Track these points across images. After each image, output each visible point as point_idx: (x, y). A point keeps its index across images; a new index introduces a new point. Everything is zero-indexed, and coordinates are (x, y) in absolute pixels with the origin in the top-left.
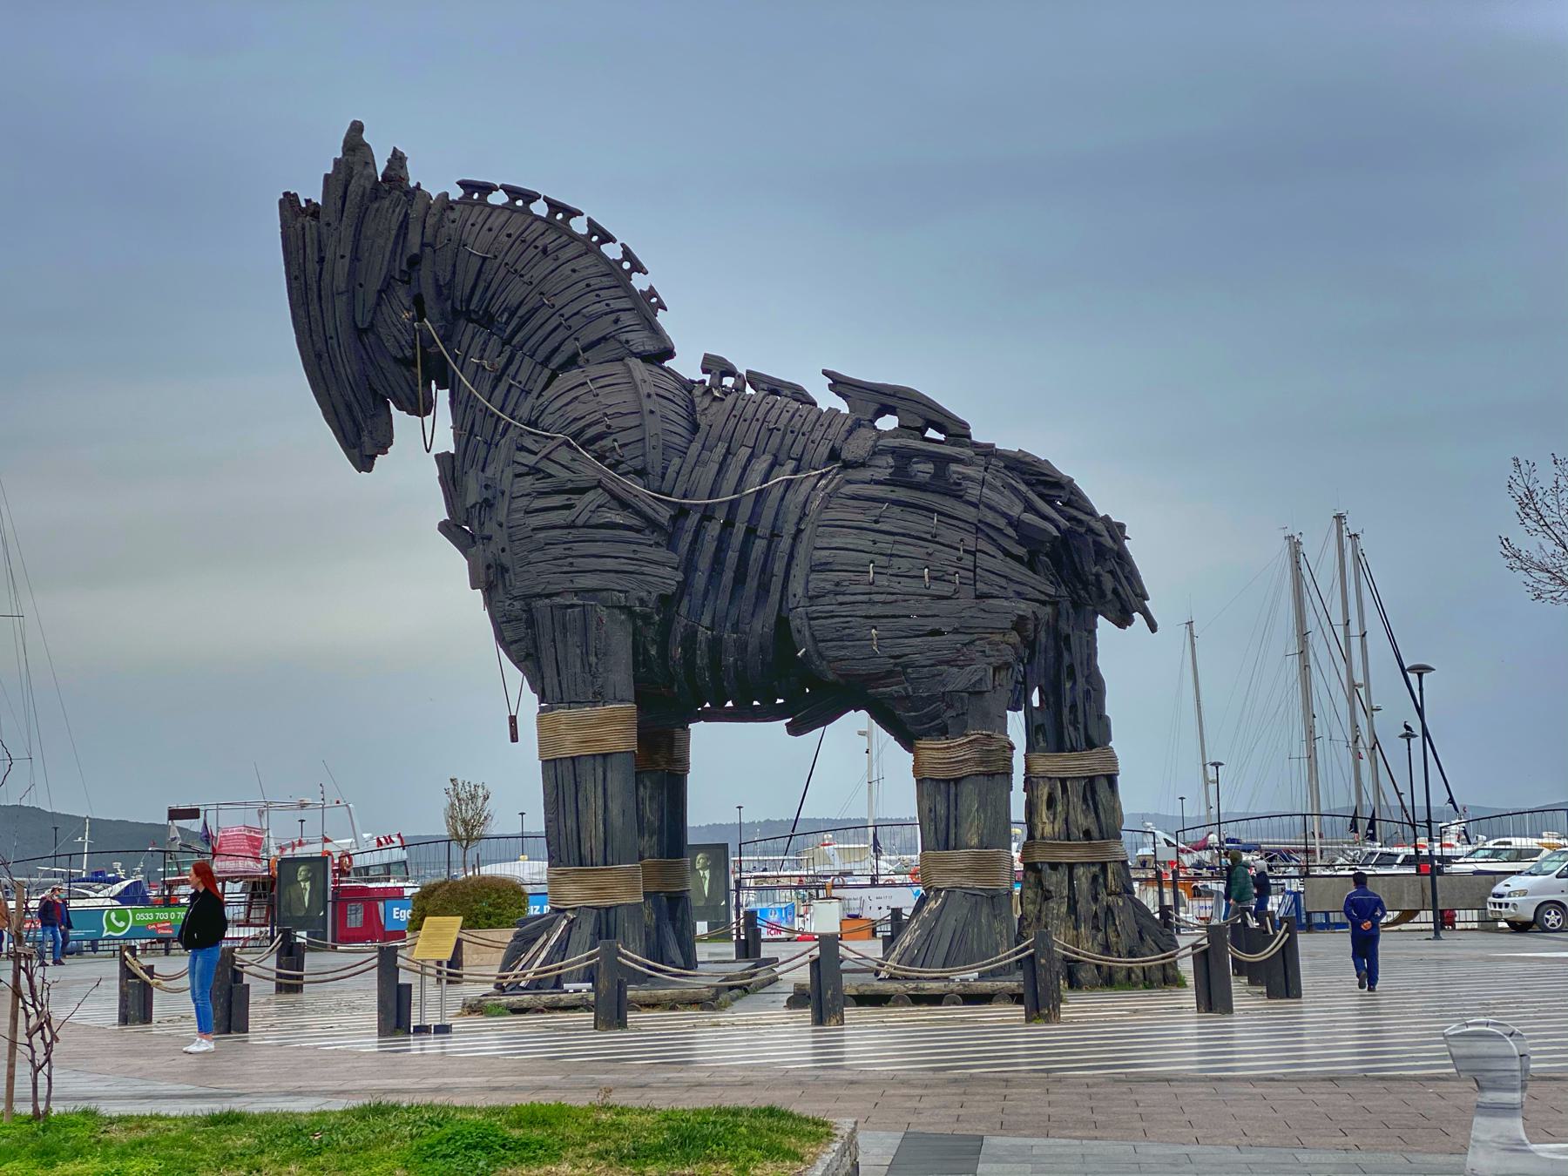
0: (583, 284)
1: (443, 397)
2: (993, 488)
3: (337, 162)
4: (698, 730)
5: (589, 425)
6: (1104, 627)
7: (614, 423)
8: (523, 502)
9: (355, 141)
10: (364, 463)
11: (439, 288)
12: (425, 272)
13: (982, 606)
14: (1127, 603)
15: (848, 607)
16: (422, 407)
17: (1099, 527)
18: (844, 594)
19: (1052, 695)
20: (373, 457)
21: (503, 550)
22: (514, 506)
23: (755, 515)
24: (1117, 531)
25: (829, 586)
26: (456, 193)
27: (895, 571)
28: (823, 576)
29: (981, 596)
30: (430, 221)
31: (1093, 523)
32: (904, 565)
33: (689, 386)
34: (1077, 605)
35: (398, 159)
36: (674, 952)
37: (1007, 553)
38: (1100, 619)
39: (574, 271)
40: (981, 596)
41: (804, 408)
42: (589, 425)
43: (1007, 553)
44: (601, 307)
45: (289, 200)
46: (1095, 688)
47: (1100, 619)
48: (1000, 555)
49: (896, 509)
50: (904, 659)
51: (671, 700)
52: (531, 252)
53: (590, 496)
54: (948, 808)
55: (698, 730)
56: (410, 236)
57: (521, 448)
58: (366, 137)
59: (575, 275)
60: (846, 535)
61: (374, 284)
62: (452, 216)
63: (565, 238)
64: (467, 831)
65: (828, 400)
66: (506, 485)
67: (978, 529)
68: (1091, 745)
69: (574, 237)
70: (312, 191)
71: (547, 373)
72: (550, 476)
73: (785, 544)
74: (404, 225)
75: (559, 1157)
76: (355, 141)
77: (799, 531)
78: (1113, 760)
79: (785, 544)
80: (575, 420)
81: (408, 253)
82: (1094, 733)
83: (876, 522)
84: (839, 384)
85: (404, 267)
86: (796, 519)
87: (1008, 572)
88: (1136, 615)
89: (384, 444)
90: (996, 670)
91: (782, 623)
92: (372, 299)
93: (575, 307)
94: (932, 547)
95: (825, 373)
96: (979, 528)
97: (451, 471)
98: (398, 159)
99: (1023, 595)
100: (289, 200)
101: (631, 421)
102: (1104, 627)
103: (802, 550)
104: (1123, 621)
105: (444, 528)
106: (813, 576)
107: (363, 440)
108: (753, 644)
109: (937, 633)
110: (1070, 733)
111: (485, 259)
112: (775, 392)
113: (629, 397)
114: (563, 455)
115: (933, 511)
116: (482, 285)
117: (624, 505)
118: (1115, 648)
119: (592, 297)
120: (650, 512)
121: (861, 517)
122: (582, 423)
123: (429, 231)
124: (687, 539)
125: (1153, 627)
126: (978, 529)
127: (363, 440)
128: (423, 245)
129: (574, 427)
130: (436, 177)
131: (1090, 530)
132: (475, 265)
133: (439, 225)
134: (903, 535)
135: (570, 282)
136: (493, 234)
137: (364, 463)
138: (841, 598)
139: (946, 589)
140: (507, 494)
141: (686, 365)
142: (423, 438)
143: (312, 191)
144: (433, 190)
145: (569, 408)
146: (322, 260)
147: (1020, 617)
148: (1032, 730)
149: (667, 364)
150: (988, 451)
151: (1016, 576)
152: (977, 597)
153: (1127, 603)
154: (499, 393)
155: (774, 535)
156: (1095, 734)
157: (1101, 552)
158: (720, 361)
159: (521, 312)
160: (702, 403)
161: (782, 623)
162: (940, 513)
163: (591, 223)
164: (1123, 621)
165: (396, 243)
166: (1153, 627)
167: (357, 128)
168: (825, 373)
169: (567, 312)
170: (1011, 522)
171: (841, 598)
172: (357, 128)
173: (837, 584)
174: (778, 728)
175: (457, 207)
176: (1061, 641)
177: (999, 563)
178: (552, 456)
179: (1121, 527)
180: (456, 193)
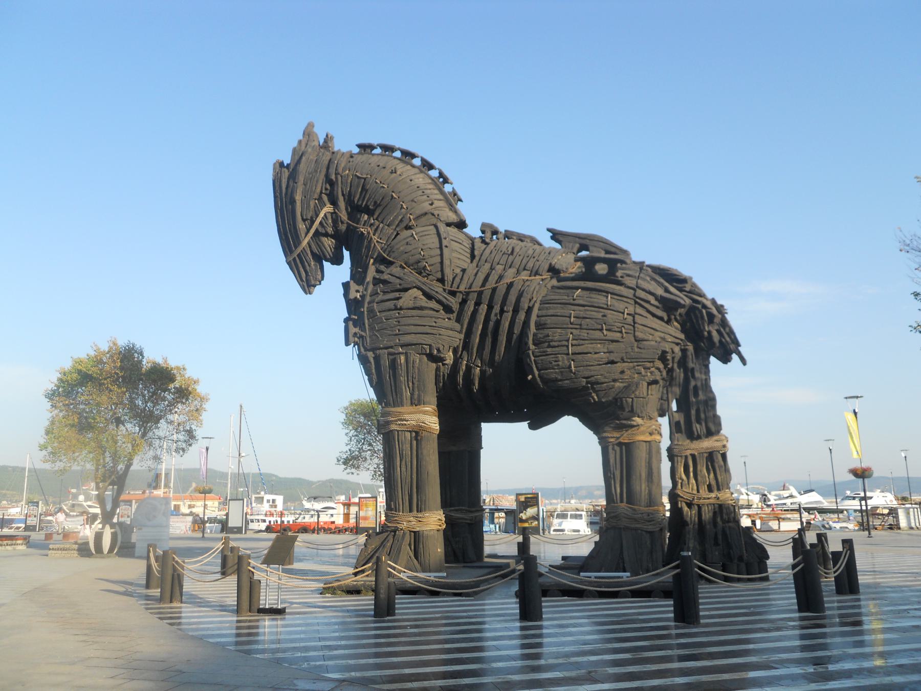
1: (346, 254)
2: (644, 280)
4: (485, 426)
6: (714, 363)
14: (727, 348)
17: (709, 304)
19: (684, 405)
24: (720, 309)
26: (356, 150)
31: (704, 301)
33: (472, 240)
34: (697, 350)
37: (654, 315)
38: (713, 359)
41: (536, 246)
46: (710, 402)
47: (713, 359)
50: (592, 379)
51: (467, 408)
54: (622, 466)
55: (485, 426)
60: (555, 308)
65: (547, 242)
68: (710, 433)
76: (308, 133)
82: (713, 428)
84: (556, 236)
90: (649, 384)
95: (549, 230)
96: (637, 301)
98: (328, 139)
99: (668, 336)
102: (714, 363)
104: (725, 359)
110: (697, 428)
115: (607, 292)
118: (721, 377)
120: (444, 300)
125: (744, 362)
126: (636, 302)
127: (308, 283)
130: (345, 144)
131: (704, 306)
141: (474, 230)
144: (344, 150)
148: (675, 428)
149: (464, 230)
150: (641, 265)
153: (727, 348)
156: (713, 427)
157: (711, 317)
160: (479, 245)
162: (612, 294)
164: (725, 359)
166: (744, 362)
167: (310, 125)
168: (549, 230)
175: (355, 156)
176: (689, 374)
179: (722, 306)
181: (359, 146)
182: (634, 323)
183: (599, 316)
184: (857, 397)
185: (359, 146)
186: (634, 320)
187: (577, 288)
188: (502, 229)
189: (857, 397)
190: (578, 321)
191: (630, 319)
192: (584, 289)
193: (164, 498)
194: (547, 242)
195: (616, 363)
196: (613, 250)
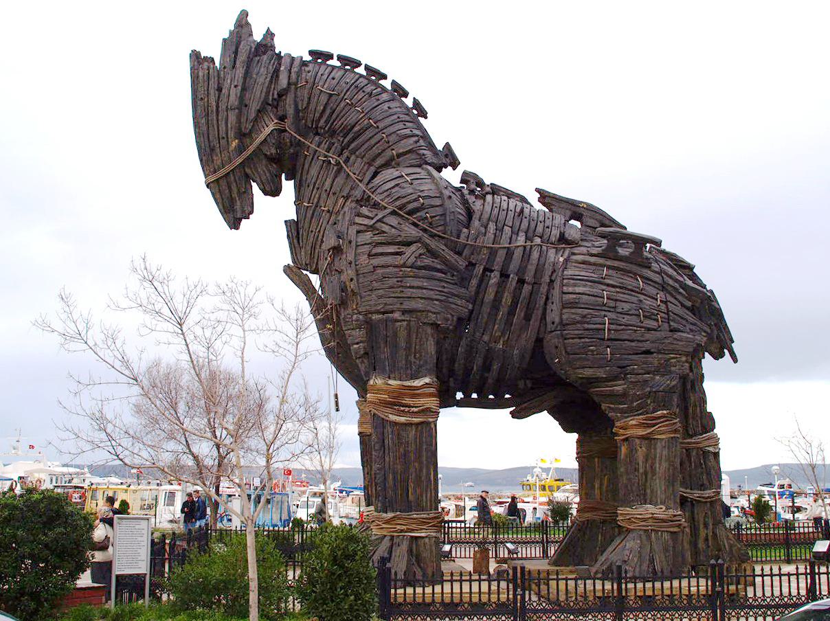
0: (396, 117)
3: (231, 33)
5: (409, 202)
8: (366, 249)
9: (242, 23)
10: (234, 224)
11: (297, 111)
12: (289, 99)
13: (675, 336)
15: (591, 332)
16: (273, 190)
18: (588, 323)
20: (240, 220)
21: (352, 280)
22: (359, 251)
23: (522, 270)
25: (578, 318)
26: (307, 58)
27: (620, 310)
28: (573, 311)
29: (673, 330)
30: (294, 70)
32: (626, 307)
35: (269, 35)
39: (389, 108)
40: (673, 330)
42: (409, 202)
43: (683, 305)
44: (407, 132)
45: (196, 56)
48: (679, 305)
52: (361, 95)
53: (413, 248)
55: (546, 412)
56: (281, 77)
57: (359, 215)
58: (249, 19)
61: (254, 106)
62: (307, 69)
63: (379, 89)
64: (167, 441)
65: (533, 198)
66: (353, 238)
69: (384, 89)
70: (213, 50)
72: (384, 232)
73: (544, 289)
74: (276, 72)
76: (242, 23)
77: (552, 281)
78: (716, 441)
79: (544, 289)
81: (279, 88)
84: (544, 197)
85: (276, 96)
86: (550, 274)
89: (248, 213)
91: (539, 341)
92: (252, 115)
93: (391, 129)
94: (642, 297)
97: (295, 231)
98: (269, 35)
100: (196, 56)
101: (438, 202)
103: (556, 292)
105: (287, 270)
106: (565, 311)
107: (235, 210)
108: (161, 373)
109: (648, 352)
111: (331, 95)
113: (433, 187)
114: (393, 221)
116: (328, 112)
119: (401, 126)
121: (593, 275)
122: (404, 201)
123: (294, 76)
124: (474, 282)
125: (735, 360)
127: (235, 210)
128: (289, 84)
129: (398, 203)
132: (324, 99)
133: (299, 74)
134: (620, 288)
135: (388, 113)
136: (335, 82)
137: (234, 224)
138: (586, 326)
139: (651, 324)
140: (353, 244)
142: (275, 210)
143: (213, 50)
145: (393, 191)
146: (220, 90)
147: (698, 345)
152: (671, 331)
155: (536, 283)
158: (475, 176)
159: (356, 129)
161: (539, 341)
163: (394, 83)
165: (271, 82)
166: (735, 360)
167: (244, 14)
168: (538, 190)
171: (586, 326)
172: (244, 14)
173: (584, 316)
177: (678, 310)
178: (385, 220)
180: (307, 58)
181: (311, 53)
182: (668, 311)
183: (634, 299)
184: (336, 396)
185: (311, 53)
186: (667, 307)
187: (602, 266)
188: (487, 182)
189: (336, 396)
190: (612, 304)
191: (663, 307)
192: (609, 267)
193: (189, 537)
194: (533, 198)
195: (652, 353)
196: (607, 222)
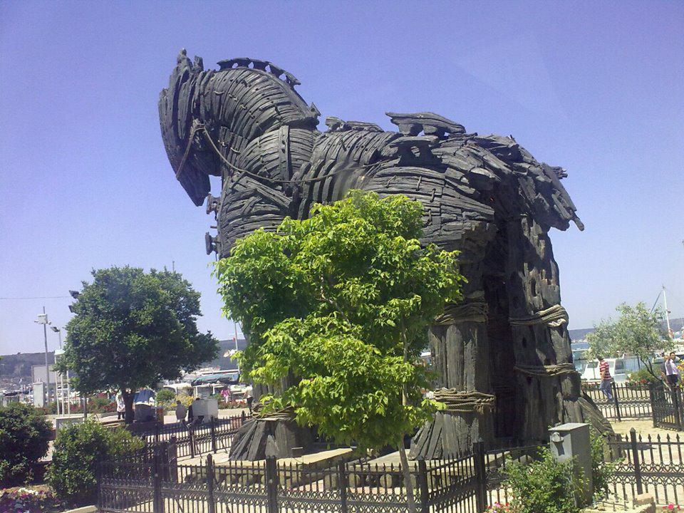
6: (553, 233)
7: (265, 159)
36: (160, 510)
49: (399, 178)
59: (257, 92)
67: (446, 182)
71: (247, 141)
75: (422, 395)
80: (250, 161)
83: (387, 187)
84: (395, 119)
87: (461, 204)
88: (571, 222)
93: (256, 107)
102: (553, 233)
112: (361, 129)
117: (269, 201)
119: (265, 100)
121: (381, 186)
125: (582, 228)
151: (468, 206)
154: (229, 156)
164: (563, 226)
166: (582, 228)
169: (252, 109)
170: (468, 174)
174: (564, 245)
